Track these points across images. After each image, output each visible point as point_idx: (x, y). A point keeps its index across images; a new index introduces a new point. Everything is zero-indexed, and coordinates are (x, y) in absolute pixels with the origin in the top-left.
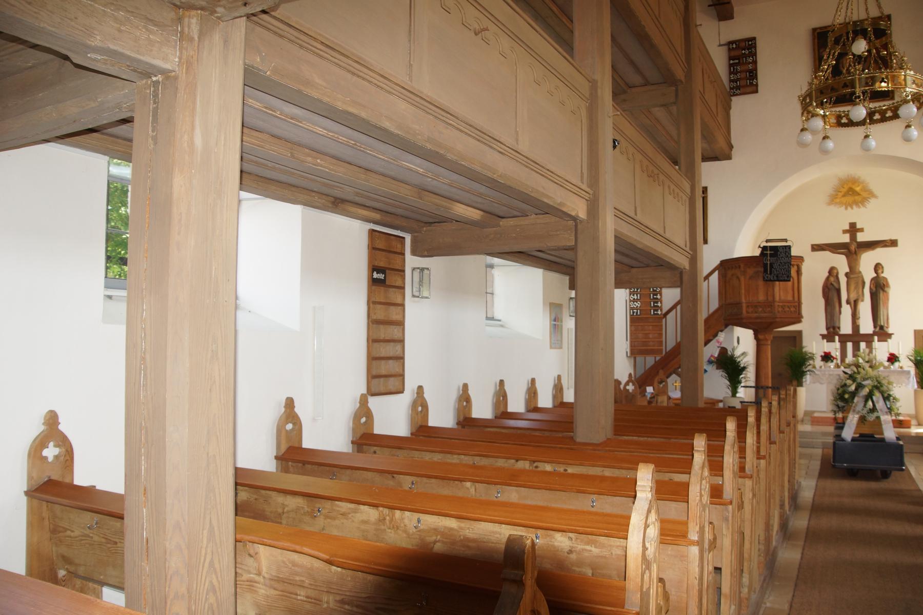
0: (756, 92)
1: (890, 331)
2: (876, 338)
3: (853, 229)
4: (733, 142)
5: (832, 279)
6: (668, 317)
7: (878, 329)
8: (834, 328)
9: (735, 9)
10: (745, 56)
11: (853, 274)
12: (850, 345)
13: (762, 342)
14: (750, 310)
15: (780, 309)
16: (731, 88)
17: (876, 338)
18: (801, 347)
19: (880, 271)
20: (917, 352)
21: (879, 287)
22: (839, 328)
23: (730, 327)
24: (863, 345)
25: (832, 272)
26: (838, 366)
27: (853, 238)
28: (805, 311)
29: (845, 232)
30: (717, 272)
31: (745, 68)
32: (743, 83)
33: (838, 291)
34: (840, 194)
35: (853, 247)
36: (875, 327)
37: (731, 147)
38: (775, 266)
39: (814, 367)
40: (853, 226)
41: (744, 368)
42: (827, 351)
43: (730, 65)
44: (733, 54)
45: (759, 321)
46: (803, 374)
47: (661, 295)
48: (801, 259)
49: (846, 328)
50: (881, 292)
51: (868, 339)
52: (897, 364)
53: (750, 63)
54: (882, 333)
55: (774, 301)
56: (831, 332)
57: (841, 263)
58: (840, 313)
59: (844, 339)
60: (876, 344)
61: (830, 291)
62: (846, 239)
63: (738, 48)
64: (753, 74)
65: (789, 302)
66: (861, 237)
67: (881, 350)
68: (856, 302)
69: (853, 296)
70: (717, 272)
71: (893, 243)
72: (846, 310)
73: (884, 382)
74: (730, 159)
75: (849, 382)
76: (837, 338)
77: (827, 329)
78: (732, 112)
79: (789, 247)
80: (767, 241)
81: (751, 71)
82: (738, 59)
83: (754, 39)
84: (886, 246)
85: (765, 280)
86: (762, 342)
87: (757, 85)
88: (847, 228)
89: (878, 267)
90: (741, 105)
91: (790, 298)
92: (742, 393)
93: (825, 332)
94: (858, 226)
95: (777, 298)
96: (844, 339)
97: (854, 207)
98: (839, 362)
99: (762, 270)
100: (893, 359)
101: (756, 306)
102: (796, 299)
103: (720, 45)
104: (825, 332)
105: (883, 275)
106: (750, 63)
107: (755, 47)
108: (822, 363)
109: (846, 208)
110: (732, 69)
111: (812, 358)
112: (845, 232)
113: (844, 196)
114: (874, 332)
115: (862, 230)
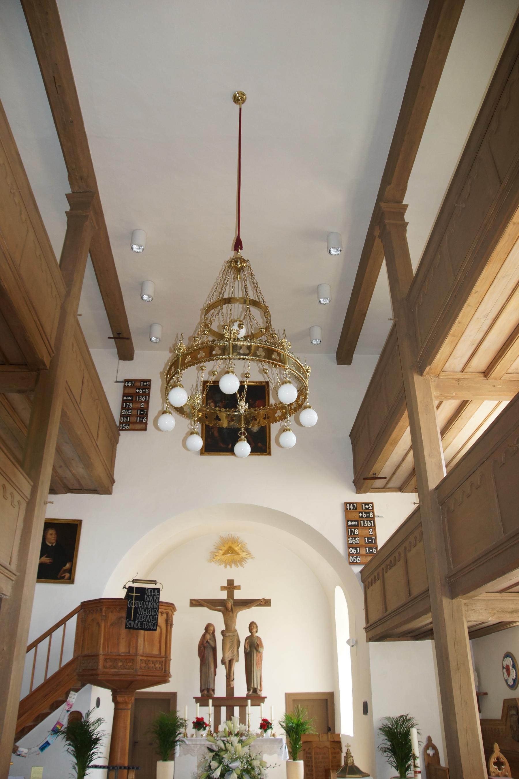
0: (145, 430)
1: (263, 694)
2: (249, 701)
3: (231, 586)
4: (115, 477)
5: (208, 637)
7: (251, 692)
8: (208, 690)
9: (136, 352)
11: (229, 632)
12: (223, 709)
13: (121, 706)
15: (143, 665)
16: (120, 423)
17: (249, 701)
18: (175, 711)
19: (254, 630)
20: (288, 718)
21: (253, 647)
22: (213, 690)
23: (88, 685)
24: (237, 709)
26: (210, 734)
27: (231, 594)
28: (175, 667)
29: (223, 588)
30: (75, 617)
31: (137, 406)
32: (133, 419)
33: (214, 649)
34: (221, 553)
35: (230, 604)
36: (249, 690)
37: (113, 481)
38: (140, 611)
39: (185, 736)
40: (230, 582)
41: (97, 740)
42: (199, 716)
43: (123, 401)
44: (127, 391)
45: (117, 678)
46: (172, 745)
48: (171, 606)
49: (220, 691)
50: (255, 652)
51: (242, 702)
52: (269, 731)
53: (142, 402)
54: (255, 697)
55: (136, 655)
57: (217, 619)
58: (215, 674)
59: (218, 703)
60: (250, 709)
61: (206, 649)
62: (223, 595)
63: (133, 386)
64: (144, 413)
65: (154, 656)
66: (238, 595)
67: (255, 714)
68: (231, 662)
69: (228, 656)
70: (75, 617)
71: (267, 603)
72: (221, 670)
73: (256, 763)
74: (110, 493)
75: (214, 764)
76: (210, 701)
77: (202, 691)
78: (118, 446)
79: (158, 590)
80: (134, 581)
81: (142, 410)
82: (132, 397)
84: (260, 605)
85: (127, 627)
88: (225, 584)
89: (252, 626)
90: (127, 440)
91: (156, 652)
93: (199, 695)
94: (236, 584)
95: (141, 651)
96: (218, 703)
97: (233, 565)
98: (212, 729)
99: (124, 615)
100: (265, 725)
101: (115, 660)
102: (163, 654)
103: (117, 382)
104: (199, 695)
105: (257, 634)
106: (142, 402)
107: (149, 389)
108: (194, 731)
109: (226, 567)
110: (125, 405)
111: (183, 725)
112: (223, 588)
113: (223, 554)
114: (247, 694)
115: (239, 588)
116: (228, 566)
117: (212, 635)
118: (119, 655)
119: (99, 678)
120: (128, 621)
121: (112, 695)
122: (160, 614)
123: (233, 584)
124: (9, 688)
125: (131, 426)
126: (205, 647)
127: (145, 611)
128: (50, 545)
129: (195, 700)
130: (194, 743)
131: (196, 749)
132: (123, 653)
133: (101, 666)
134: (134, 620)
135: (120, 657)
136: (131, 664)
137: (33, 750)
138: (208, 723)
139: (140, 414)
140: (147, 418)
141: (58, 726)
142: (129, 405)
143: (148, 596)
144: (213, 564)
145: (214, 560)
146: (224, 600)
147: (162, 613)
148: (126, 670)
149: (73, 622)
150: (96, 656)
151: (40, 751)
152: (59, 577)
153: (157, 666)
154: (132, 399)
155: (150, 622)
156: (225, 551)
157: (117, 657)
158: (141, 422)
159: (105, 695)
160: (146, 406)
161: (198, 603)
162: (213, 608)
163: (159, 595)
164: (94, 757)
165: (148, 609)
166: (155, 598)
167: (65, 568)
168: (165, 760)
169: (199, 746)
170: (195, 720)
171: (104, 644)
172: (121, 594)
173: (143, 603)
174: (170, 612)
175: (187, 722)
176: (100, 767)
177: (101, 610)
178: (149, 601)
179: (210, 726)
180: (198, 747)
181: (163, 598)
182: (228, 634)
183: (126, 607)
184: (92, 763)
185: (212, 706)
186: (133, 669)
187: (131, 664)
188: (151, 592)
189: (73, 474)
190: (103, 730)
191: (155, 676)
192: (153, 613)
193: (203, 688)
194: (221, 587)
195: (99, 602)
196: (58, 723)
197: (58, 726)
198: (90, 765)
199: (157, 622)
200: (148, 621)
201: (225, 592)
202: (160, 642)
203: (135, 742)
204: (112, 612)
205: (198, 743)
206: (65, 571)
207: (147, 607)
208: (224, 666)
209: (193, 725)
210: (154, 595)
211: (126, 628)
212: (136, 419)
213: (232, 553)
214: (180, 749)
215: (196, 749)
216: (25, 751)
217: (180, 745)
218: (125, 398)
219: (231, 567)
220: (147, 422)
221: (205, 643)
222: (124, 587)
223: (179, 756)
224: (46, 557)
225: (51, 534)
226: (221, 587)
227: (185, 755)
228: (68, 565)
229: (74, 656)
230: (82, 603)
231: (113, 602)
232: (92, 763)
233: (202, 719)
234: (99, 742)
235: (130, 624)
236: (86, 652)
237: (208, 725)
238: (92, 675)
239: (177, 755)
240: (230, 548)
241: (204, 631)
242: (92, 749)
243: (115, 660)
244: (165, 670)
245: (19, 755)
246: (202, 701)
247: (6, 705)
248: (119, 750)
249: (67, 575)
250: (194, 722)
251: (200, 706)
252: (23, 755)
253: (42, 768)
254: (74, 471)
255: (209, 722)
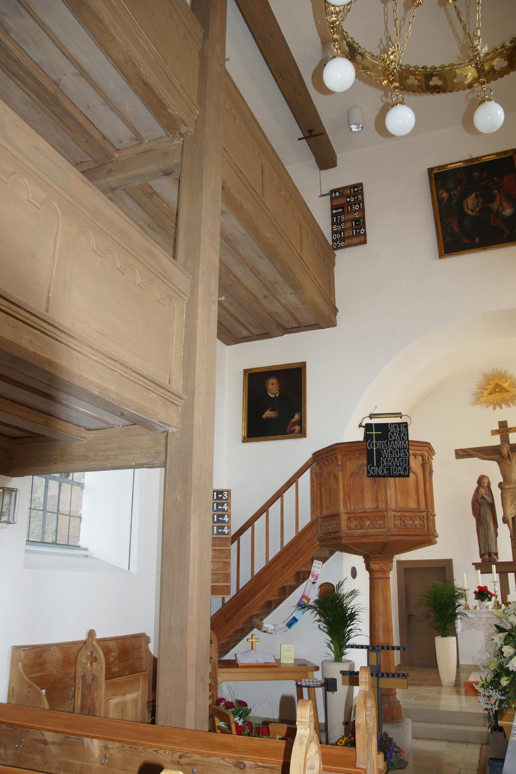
0: (365, 242)
4: (337, 305)
5: (483, 491)
6: (242, 538)
8: (490, 554)
10: (350, 204)
14: (354, 524)
15: (398, 522)
16: (333, 241)
18: (452, 580)
22: (496, 554)
23: (338, 553)
25: (482, 482)
26: (498, 606)
27: (505, 439)
28: (441, 525)
29: (494, 433)
30: (308, 473)
31: (351, 216)
32: (348, 233)
33: (492, 506)
34: (486, 392)
35: (505, 450)
38: (384, 454)
39: (467, 608)
40: (503, 425)
41: (352, 617)
43: (333, 215)
44: (336, 203)
45: (365, 540)
46: (454, 616)
47: (229, 505)
48: (427, 448)
53: (355, 211)
56: (487, 561)
57: (492, 471)
58: (497, 535)
59: (504, 569)
62: (496, 441)
63: (342, 195)
64: (360, 223)
70: (308, 473)
74: (334, 325)
76: (494, 567)
77: (482, 556)
80: (371, 416)
81: (357, 220)
82: (343, 208)
83: (361, 185)
86: (377, 575)
87: (365, 235)
88: (497, 428)
90: (345, 259)
91: (412, 505)
92: (351, 654)
93: (479, 560)
95: (392, 505)
98: (499, 599)
99: (365, 461)
101: (361, 519)
103: (322, 196)
104: (479, 560)
106: (355, 211)
107: (362, 194)
108: (477, 602)
109: (494, 408)
111: (463, 595)
112: (494, 433)
113: (490, 394)
116: (498, 408)
117: (487, 489)
118: (365, 512)
119: (344, 541)
120: (370, 468)
121: (365, 562)
122: (412, 458)
123: (507, 426)
124: (189, 551)
125: (347, 242)
126: (480, 504)
127: (391, 452)
128: (273, 396)
129: (474, 566)
130: (478, 616)
131: (482, 623)
132: (370, 509)
133: (344, 527)
134: (378, 465)
135: (367, 515)
136: (381, 522)
137: (279, 626)
138: (493, 593)
139: (356, 225)
140: (365, 228)
141: (304, 600)
142: (341, 218)
143: (393, 433)
144: (478, 407)
145: (479, 402)
146: (497, 446)
147: (415, 455)
148: (376, 530)
149: (305, 479)
150: (337, 515)
151: (287, 628)
152: (287, 431)
153: (416, 522)
154: (343, 210)
155: (400, 466)
156: (492, 390)
157: (362, 515)
158: (358, 234)
159: (358, 561)
160: (361, 215)
161: (465, 454)
162: (485, 457)
163: (407, 430)
164: (352, 635)
165: (395, 450)
166: (402, 435)
167: (293, 420)
168: (444, 635)
169: (484, 620)
170: (477, 590)
171: (344, 500)
172: (359, 435)
173: (387, 443)
174: (426, 454)
175: (467, 592)
176: (362, 647)
177: (336, 458)
178: (395, 440)
179: (496, 596)
180: (484, 621)
181: (413, 435)
182: (507, 487)
183: (366, 452)
184: (350, 642)
185: (497, 573)
186: (385, 528)
187: (381, 522)
188: (396, 427)
189: (284, 306)
190: (360, 603)
191: (415, 535)
192: (402, 454)
193: (483, 552)
194: (492, 431)
195: (332, 450)
196: (303, 596)
197: (304, 600)
198: (347, 644)
199: (409, 465)
200: (396, 465)
201: (498, 438)
202: (417, 493)
203: (410, 615)
204: (349, 460)
205: (483, 616)
206: (294, 424)
207: (393, 448)
208: (506, 524)
209: (474, 595)
210: (400, 431)
211: (368, 476)
212: (351, 231)
213: (500, 391)
214: (462, 623)
215: (482, 623)
216: (271, 627)
217: (461, 619)
218: (334, 211)
219: (501, 408)
220: (365, 232)
221: (479, 499)
222: (360, 426)
223: (462, 630)
224: (271, 411)
225: (273, 384)
226: (492, 431)
227: (468, 629)
228: (297, 417)
229: (312, 518)
230: (313, 454)
231: (348, 447)
232: (350, 642)
233: (486, 587)
234: (356, 617)
235: (373, 470)
236: (325, 513)
237: (494, 595)
238: (335, 539)
239: (459, 630)
240: (497, 385)
241: (477, 485)
242: (349, 625)
243: (361, 519)
244: (428, 528)
245: (265, 632)
246: (484, 567)
247: (188, 572)
248: (381, 627)
249: (297, 428)
250: (475, 592)
251: (481, 573)
252: (269, 631)
253: (293, 645)
254: (283, 301)
255: (495, 591)
